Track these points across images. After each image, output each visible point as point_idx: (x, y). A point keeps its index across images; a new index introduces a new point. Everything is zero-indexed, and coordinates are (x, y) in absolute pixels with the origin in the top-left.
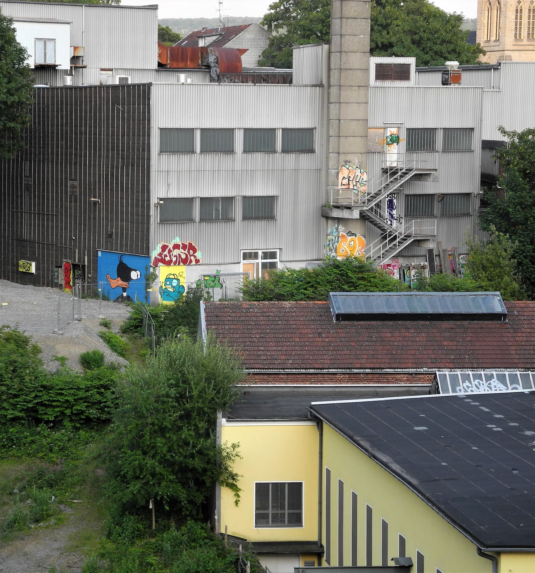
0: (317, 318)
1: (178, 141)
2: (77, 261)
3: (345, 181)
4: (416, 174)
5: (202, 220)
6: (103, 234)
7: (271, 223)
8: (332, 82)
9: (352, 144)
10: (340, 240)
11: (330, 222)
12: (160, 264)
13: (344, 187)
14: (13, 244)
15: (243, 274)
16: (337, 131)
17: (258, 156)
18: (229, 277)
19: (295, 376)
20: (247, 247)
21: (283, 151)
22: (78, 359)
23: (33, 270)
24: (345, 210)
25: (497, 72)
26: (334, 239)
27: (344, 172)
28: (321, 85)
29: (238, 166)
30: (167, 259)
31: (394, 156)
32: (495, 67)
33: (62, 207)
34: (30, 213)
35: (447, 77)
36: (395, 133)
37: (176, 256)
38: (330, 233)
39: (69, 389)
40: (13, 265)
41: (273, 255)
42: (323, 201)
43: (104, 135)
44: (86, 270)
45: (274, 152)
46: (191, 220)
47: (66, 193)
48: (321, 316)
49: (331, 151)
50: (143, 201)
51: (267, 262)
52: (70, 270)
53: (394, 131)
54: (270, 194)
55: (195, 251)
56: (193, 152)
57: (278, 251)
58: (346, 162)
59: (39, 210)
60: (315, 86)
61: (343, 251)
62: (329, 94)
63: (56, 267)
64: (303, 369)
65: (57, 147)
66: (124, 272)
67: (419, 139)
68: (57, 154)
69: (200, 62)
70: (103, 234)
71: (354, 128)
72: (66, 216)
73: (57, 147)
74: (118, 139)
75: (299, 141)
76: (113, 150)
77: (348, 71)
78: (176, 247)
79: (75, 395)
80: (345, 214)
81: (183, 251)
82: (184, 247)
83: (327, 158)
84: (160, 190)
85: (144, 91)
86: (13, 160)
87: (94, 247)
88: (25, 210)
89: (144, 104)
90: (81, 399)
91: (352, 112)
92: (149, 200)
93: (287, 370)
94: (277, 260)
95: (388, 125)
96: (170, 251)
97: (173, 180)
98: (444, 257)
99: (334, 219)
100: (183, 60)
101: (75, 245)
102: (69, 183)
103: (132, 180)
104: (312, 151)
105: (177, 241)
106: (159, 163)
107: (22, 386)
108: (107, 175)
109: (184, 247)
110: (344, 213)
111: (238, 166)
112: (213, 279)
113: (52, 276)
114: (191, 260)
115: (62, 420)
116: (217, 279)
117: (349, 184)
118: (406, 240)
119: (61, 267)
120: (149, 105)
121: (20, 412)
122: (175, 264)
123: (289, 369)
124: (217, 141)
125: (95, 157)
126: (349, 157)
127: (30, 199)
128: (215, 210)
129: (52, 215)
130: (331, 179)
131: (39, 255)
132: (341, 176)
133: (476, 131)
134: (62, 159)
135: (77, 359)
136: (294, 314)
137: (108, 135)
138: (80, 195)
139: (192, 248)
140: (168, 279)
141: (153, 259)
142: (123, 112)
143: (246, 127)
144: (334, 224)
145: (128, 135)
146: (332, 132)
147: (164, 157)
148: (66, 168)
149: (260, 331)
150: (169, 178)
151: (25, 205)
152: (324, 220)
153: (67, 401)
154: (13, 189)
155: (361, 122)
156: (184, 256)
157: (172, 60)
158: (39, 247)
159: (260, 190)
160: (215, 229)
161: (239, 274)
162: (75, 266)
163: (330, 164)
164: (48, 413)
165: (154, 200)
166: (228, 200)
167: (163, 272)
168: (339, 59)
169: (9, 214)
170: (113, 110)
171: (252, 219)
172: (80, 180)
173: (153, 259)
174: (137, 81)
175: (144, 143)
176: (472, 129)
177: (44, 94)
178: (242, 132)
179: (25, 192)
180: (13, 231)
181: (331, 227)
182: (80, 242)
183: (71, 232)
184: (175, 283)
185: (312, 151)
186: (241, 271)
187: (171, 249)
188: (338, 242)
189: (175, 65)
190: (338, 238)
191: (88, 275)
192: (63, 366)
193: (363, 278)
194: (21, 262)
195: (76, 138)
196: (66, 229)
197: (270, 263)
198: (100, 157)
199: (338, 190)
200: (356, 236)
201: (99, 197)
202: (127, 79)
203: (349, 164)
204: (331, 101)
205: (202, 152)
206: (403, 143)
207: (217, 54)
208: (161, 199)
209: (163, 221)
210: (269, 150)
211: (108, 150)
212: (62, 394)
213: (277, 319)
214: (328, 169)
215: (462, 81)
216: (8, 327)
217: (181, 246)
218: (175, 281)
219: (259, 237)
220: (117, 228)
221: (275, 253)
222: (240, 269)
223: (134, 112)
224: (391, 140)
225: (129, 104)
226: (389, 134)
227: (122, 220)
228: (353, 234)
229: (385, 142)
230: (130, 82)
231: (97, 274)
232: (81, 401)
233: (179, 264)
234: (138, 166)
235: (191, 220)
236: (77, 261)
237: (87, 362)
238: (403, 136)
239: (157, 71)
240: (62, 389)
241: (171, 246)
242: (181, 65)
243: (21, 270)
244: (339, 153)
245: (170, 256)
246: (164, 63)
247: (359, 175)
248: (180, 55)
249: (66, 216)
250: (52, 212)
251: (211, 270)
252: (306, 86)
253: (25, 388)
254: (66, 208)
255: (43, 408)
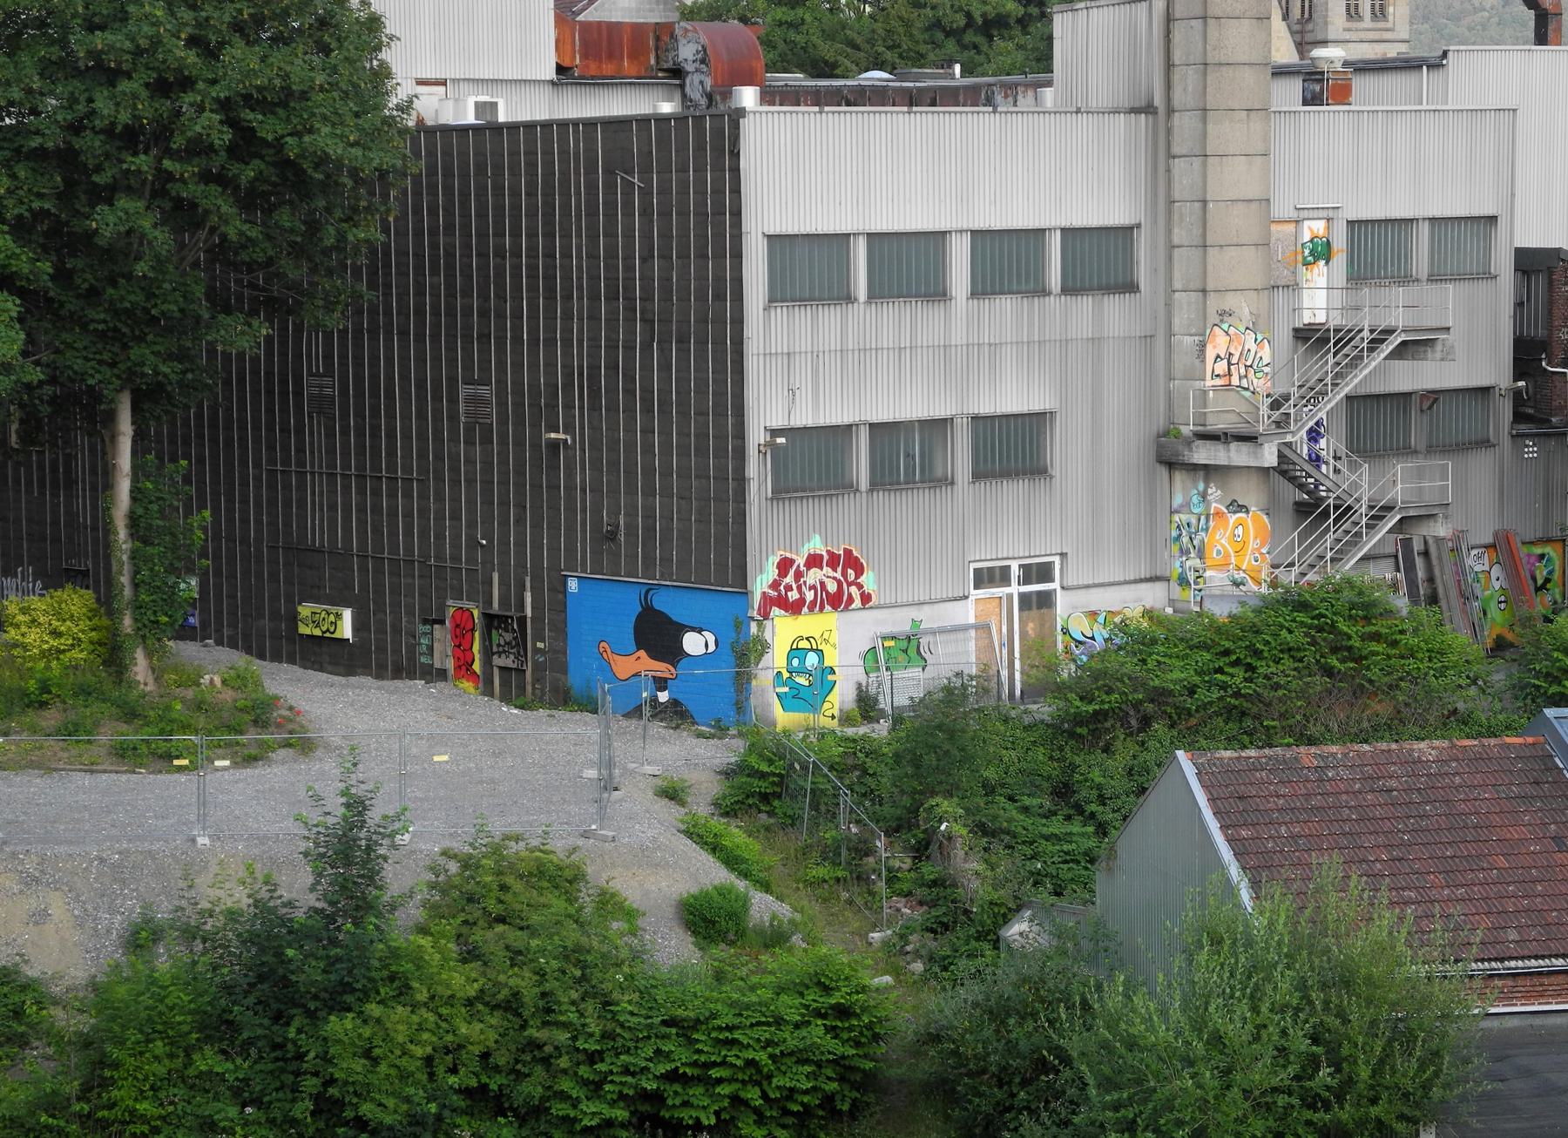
0: (1530, 790)
1: (812, 268)
2: (496, 605)
3: (1221, 367)
4: (1404, 343)
5: (875, 485)
6: (584, 531)
7: (1041, 484)
8: (1178, 98)
9: (1235, 267)
10: (1211, 524)
11: (1179, 477)
12: (776, 611)
13: (1218, 382)
14: (274, 562)
15: (976, 627)
16: (1197, 232)
17: (1006, 305)
18: (944, 637)
19: (1536, 980)
20: (984, 555)
21: (1067, 290)
22: (673, 910)
23: (346, 630)
24: (1234, 445)
25: (1437, 75)
26: (1194, 521)
27: (1218, 344)
28: (1149, 109)
29: (958, 336)
30: (793, 595)
31: (1319, 297)
32: (1432, 61)
33: (439, 458)
34: (332, 476)
35: (1317, 88)
36: (1321, 233)
37: (813, 587)
38: (1182, 506)
39: (752, 1025)
40: (275, 615)
41: (1042, 572)
42: (1161, 423)
43: (579, 257)
44: (529, 631)
45: (1044, 292)
46: (850, 487)
47: (454, 417)
48: (1537, 783)
49: (1177, 285)
50: (721, 437)
51: (1031, 593)
52: (473, 630)
53: (1319, 227)
54: (1036, 406)
55: (859, 571)
56: (849, 299)
57: (1057, 560)
58: (1224, 314)
59: (361, 466)
60: (1134, 111)
61: (1219, 552)
62: (1169, 131)
63: (425, 622)
64: (1557, 956)
65: (420, 293)
66: (659, 636)
67: (1375, 248)
68: (420, 312)
69: (653, 62)
70: (584, 531)
71: (1231, 223)
72: (455, 483)
73: (420, 293)
74: (630, 268)
75: (1100, 262)
76: (612, 297)
77: (1224, 69)
78: (814, 561)
79: (769, 1043)
80: (1238, 455)
81: (831, 573)
82: (833, 561)
83: (1168, 305)
84: (774, 403)
85: (718, 133)
86: (343, 333)
87: (554, 566)
88: (312, 466)
89: (718, 168)
90: (791, 1054)
91: (1232, 179)
92: (740, 434)
93: (1513, 964)
94: (1055, 585)
95: (1305, 214)
96: (798, 575)
97: (802, 379)
98: (1440, 558)
99: (1194, 468)
100: (610, 56)
101: (487, 563)
102: (463, 391)
103: (683, 380)
104: (1131, 287)
105: (816, 545)
106: (768, 330)
107: (610, 1026)
108: (594, 368)
109: (833, 561)
110: (1233, 454)
111: (958, 336)
112: (904, 644)
113: (412, 649)
114: (850, 595)
115: (733, 1118)
116: (914, 643)
117: (1230, 374)
118: (1381, 518)
119: (442, 622)
120: (736, 170)
121: (613, 1104)
122: (811, 608)
123: (1516, 958)
124: (907, 266)
125: (550, 317)
126: (1230, 301)
127: (330, 435)
128: (905, 456)
129: (346, 477)
130: (1181, 361)
131: (364, 587)
132: (1210, 354)
133: (1502, 223)
134: (436, 326)
135: (670, 912)
136: (1457, 780)
137: (594, 256)
138: (503, 421)
139: (852, 562)
140: (795, 651)
141: (757, 597)
142: (646, 193)
143: (976, 227)
144: (1195, 482)
145: (666, 256)
146: (1179, 236)
147: (780, 314)
148: (451, 349)
149: (1381, 840)
150: (799, 373)
151: (312, 452)
152: (1163, 471)
153: (751, 1063)
154: (270, 411)
155: (1255, 206)
156: (832, 587)
157: (585, 56)
158: (363, 569)
159: (1012, 397)
160: (905, 510)
161: (965, 628)
162: (492, 621)
163: (1176, 321)
164: (695, 1102)
165: (756, 436)
166: (938, 427)
167: (783, 631)
168: (1198, 38)
169: (258, 479)
170: (610, 187)
171: (994, 477)
172: (501, 382)
173: (757, 597)
174: (524, 115)
175: (719, 279)
176: (1492, 220)
177: (548, 141)
178: (967, 239)
179: (311, 417)
180: (273, 524)
181: (1183, 490)
182: (505, 552)
183: (472, 525)
184: (812, 659)
185: (1131, 287)
186: (972, 620)
187: (802, 568)
188: (1207, 530)
189: (593, 68)
190: (1207, 520)
191: (534, 645)
192: (635, 935)
193: (1376, 637)
194: (305, 610)
195: (484, 267)
196: (456, 516)
197: (1039, 593)
198: (567, 316)
199: (1205, 392)
200: (1247, 512)
201: (569, 429)
202: (494, 105)
203: (1230, 320)
204: (1176, 150)
205: (872, 296)
206: (1340, 260)
207: (704, 40)
208: (775, 433)
209: (782, 491)
210: (1023, 287)
211: (594, 297)
212: (733, 1043)
213: (1415, 797)
214: (1170, 334)
215: (1352, 99)
216: (517, 839)
217: (826, 557)
218: (811, 654)
219: (1009, 526)
220: (632, 514)
221: (1050, 565)
222: (966, 613)
223: (684, 191)
224: (1311, 253)
225: (665, 170)
226: (1307, 238)
227: (649, 492)
228: (1242, 508)
229: (1300, 258)
230: (502, 119)
231: (565, 641)
232: (790, 1061)
233: (822, 609)
234: (701, 342)
235: (850, 487)
236: (496, 605)
237: (705, 920)
238: (1340, 242)
239: (552, 83)
240: (729, 1028)
241: (800, 561)
242: (608, 68)
243: (304, 630)
244: (1204, 291)
245: (799, 588)
246: (566, 64)
247: (1253, 347)
248: (604, 44)
249: (455, 483)
250: (407, 469)
251: (898, 622)
252: (1116, 112)
253: (618, 1030)
254: (455, 458)
255: (677, 1087)
